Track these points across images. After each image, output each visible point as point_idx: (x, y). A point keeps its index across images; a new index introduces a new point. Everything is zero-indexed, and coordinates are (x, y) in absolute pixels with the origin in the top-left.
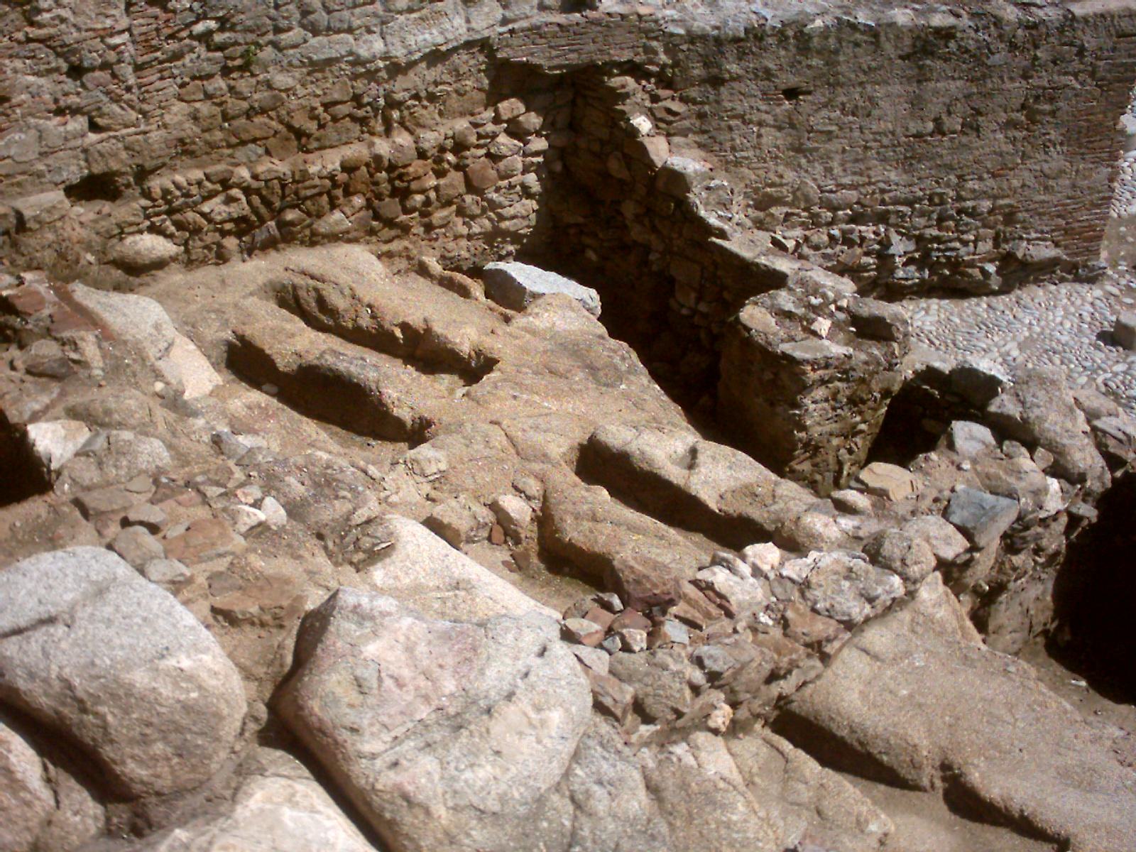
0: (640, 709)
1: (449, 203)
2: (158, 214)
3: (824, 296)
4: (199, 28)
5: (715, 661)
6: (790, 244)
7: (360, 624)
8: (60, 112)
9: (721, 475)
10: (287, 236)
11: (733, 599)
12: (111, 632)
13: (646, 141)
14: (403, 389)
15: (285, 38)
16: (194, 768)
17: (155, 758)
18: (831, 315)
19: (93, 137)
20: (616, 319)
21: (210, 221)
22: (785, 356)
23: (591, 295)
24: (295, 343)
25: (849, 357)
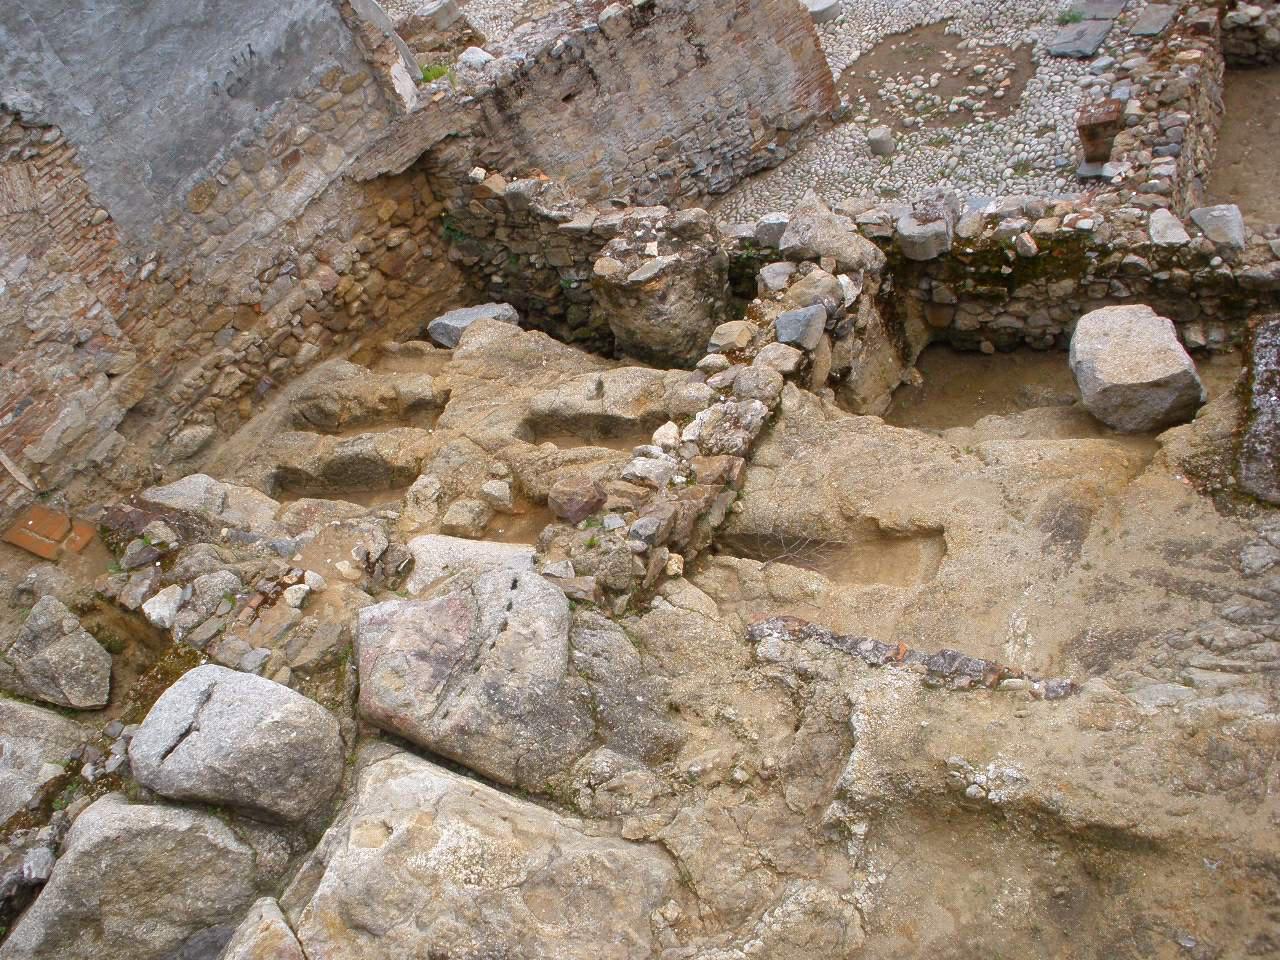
0: (607, 591)
1: (380, 295)
2: (185, 412)
3: (644, 226)
4: (144, 274)
5: (646, 527)
6: (626, 200)
7: (378, 631)
8: (84, 378)
9: (623, 387)
10: (279, 380)
11: (652, 476)
12: (224, 721)
13: (486, 183)
14: (388, 444)
15: (204, 248)
16: (322, 784)
17: (293, 790)
18: (654, 238)
19: (115, 383)
20: (529, 317)
21: (222, 397)
22: (634, 283)
23: (506, 309)
24: (312, 450)
25: (678, 261)
